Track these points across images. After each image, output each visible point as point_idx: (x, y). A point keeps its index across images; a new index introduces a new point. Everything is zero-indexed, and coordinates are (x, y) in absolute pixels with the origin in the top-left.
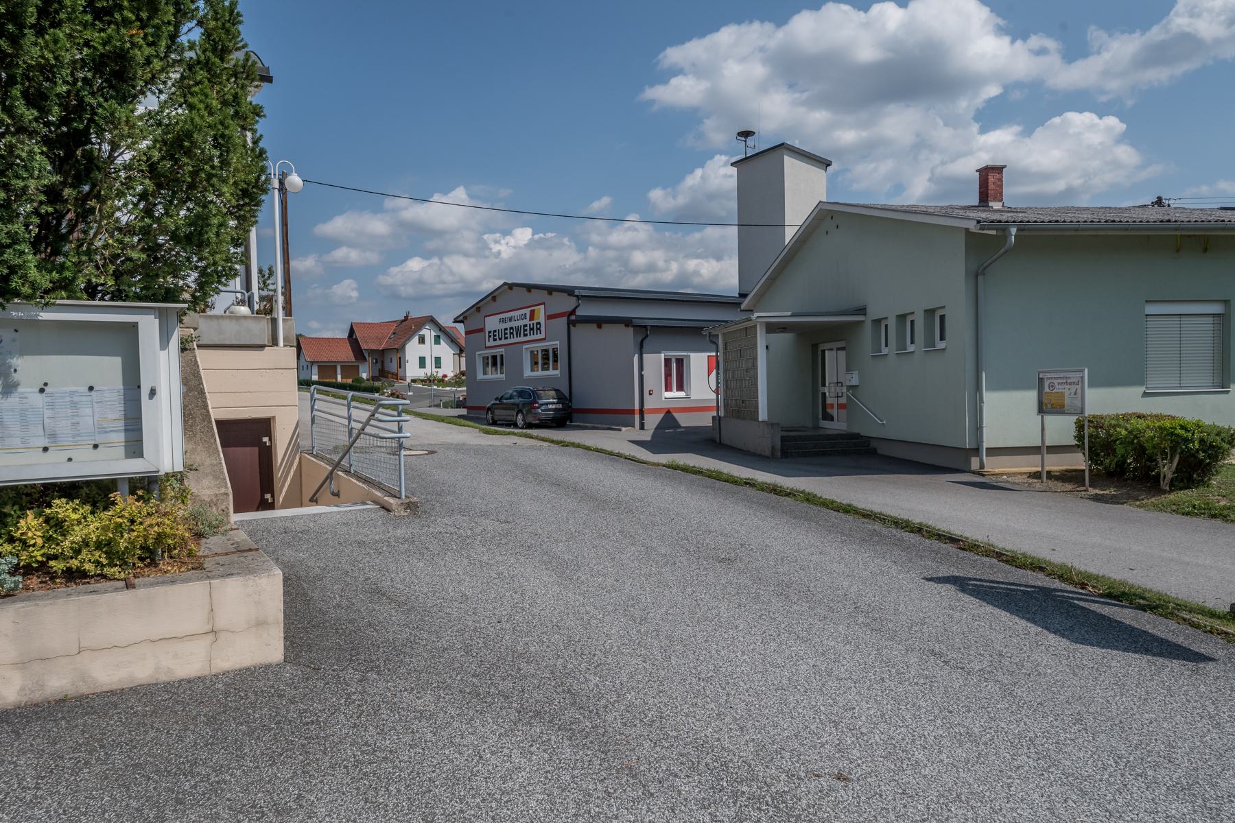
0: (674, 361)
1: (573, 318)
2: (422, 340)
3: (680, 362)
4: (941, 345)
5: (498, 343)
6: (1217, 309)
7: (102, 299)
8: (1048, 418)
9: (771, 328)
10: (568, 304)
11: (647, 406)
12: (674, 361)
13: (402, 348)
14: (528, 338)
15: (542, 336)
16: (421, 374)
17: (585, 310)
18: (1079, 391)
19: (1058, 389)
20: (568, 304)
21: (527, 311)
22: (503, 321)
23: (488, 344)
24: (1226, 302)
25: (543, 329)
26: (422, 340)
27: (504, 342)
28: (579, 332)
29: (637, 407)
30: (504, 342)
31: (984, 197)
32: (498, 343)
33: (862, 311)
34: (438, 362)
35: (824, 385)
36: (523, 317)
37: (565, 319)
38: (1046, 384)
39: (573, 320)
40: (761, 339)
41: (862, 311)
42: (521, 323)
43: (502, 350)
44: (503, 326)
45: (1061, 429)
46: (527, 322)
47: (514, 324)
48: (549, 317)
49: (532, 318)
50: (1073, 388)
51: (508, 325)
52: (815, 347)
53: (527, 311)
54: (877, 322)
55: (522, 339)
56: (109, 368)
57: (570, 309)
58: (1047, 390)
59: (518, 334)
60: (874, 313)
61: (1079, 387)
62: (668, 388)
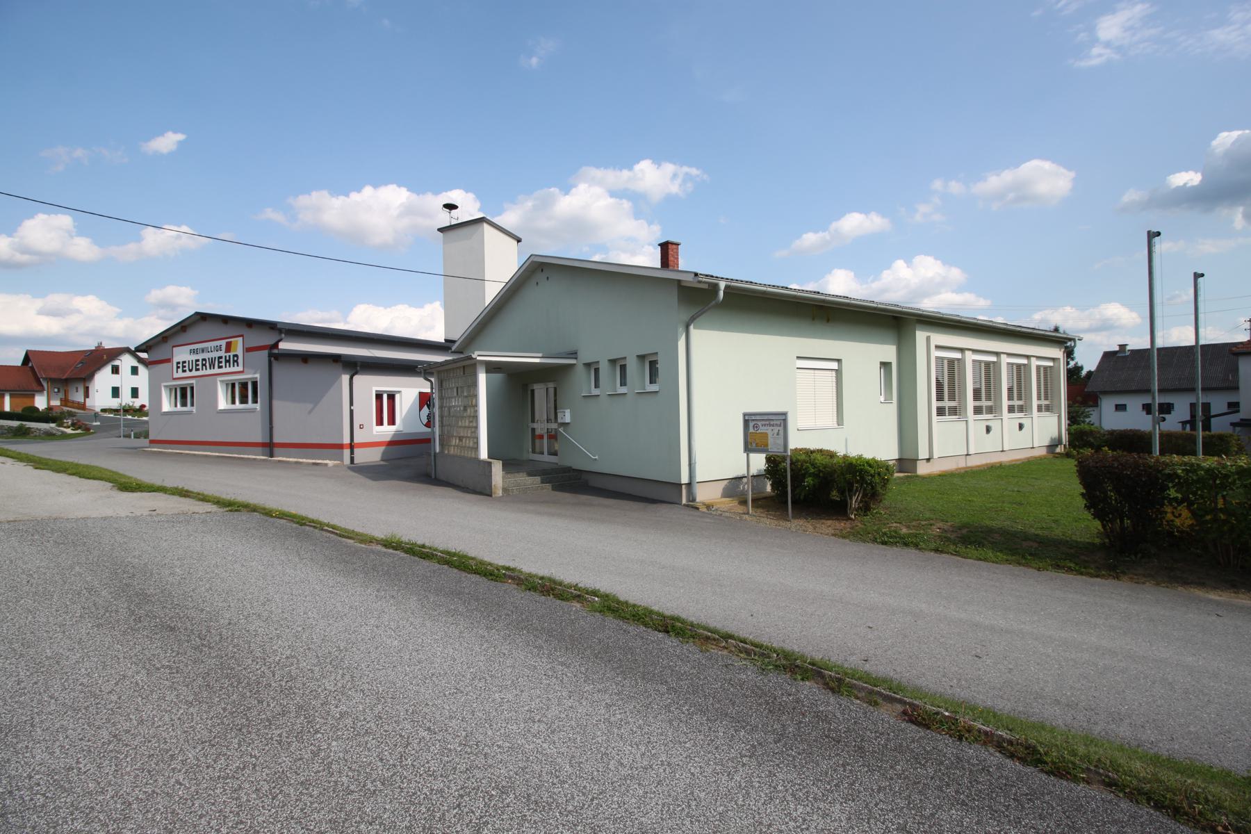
0: (385, 397)
1: (276, 351)
2: (116, 370)
3: (392, 397)
4: (654, 388)
5: (188, 374)
6: (835, 365)
7: (220, 367)
8: (752, 455)
9: (492, 368)
10: (268, 339)
11: (356, 440)
12: (385, 397)
13: (91, 377)
14: (223, 370)
15: (240, 368)
16: (114, 403)
17: (285, 346)
18: (781, 432)
19: (762, 430)
20: (268, 339)
21: (223, 343)
22: (194, 352)
23: (176, 376)
24: (839, 361)
25: (240, 361)
26: (116, 370)
27: (194, 373)
28: (280, 370)
29: (347, 441)
30: (194, 373)
31: (665, 262)
32: (188, 374)
33: (574, 354)
34: (135, 393)
35: (533, 421)
36: (219, 349)
37: (266, 352)
38: (751, 424)
39: (276, 356)
40: (482, 378)
41: (574, 354)
42: (216, 354)
43: (193, 381)
44: (194, 357)
45: (759, 462)
46: (222, 353)
47: (206, 356)
48: (248, 350)
49: (228, 350)
50: (776, 429)
51: (200, 357)
52: (525, 387)
53: (223, 343)
54: (588, 365)
55: (217, 370)
56: (888, 352)
57: (272, 342)
58: (751, 430)
59: (212, 365)
60: (585, 357)
61: (781, 429)
62: (380, 422)
